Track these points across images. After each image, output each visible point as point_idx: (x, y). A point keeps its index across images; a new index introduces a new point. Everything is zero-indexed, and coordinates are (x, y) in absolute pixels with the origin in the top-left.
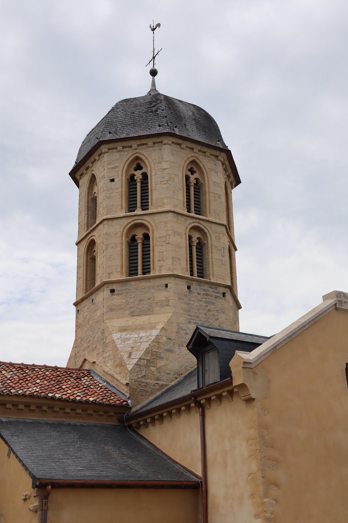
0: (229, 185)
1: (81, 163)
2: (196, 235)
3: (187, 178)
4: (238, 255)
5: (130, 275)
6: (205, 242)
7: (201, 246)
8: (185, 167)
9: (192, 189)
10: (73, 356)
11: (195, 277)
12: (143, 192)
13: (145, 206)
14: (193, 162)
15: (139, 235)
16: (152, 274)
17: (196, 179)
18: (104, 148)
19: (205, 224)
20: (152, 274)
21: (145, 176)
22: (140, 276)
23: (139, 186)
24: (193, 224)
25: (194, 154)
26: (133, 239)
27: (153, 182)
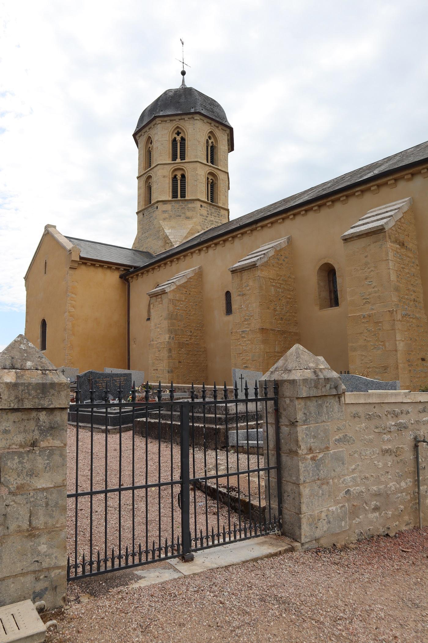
1: (140, 202)
2: (210, 177)
3: (207, 142)
5: (173, 160)
7: (213, 184)
8: (206, 135)
10: (138, 240)
11: (210, 202)
12: (181, 154)
13: (183, 157)
14: (211, 132)
16: (186, 161)
17: (212, 142)
18: (158, 121)
19: (216, 170)
20: (186, 161)
21: (183, 139)
22: (179, 198)
23: (179, 182)
24: (210, 171)
25: (212, 128)
26: (175, 178)
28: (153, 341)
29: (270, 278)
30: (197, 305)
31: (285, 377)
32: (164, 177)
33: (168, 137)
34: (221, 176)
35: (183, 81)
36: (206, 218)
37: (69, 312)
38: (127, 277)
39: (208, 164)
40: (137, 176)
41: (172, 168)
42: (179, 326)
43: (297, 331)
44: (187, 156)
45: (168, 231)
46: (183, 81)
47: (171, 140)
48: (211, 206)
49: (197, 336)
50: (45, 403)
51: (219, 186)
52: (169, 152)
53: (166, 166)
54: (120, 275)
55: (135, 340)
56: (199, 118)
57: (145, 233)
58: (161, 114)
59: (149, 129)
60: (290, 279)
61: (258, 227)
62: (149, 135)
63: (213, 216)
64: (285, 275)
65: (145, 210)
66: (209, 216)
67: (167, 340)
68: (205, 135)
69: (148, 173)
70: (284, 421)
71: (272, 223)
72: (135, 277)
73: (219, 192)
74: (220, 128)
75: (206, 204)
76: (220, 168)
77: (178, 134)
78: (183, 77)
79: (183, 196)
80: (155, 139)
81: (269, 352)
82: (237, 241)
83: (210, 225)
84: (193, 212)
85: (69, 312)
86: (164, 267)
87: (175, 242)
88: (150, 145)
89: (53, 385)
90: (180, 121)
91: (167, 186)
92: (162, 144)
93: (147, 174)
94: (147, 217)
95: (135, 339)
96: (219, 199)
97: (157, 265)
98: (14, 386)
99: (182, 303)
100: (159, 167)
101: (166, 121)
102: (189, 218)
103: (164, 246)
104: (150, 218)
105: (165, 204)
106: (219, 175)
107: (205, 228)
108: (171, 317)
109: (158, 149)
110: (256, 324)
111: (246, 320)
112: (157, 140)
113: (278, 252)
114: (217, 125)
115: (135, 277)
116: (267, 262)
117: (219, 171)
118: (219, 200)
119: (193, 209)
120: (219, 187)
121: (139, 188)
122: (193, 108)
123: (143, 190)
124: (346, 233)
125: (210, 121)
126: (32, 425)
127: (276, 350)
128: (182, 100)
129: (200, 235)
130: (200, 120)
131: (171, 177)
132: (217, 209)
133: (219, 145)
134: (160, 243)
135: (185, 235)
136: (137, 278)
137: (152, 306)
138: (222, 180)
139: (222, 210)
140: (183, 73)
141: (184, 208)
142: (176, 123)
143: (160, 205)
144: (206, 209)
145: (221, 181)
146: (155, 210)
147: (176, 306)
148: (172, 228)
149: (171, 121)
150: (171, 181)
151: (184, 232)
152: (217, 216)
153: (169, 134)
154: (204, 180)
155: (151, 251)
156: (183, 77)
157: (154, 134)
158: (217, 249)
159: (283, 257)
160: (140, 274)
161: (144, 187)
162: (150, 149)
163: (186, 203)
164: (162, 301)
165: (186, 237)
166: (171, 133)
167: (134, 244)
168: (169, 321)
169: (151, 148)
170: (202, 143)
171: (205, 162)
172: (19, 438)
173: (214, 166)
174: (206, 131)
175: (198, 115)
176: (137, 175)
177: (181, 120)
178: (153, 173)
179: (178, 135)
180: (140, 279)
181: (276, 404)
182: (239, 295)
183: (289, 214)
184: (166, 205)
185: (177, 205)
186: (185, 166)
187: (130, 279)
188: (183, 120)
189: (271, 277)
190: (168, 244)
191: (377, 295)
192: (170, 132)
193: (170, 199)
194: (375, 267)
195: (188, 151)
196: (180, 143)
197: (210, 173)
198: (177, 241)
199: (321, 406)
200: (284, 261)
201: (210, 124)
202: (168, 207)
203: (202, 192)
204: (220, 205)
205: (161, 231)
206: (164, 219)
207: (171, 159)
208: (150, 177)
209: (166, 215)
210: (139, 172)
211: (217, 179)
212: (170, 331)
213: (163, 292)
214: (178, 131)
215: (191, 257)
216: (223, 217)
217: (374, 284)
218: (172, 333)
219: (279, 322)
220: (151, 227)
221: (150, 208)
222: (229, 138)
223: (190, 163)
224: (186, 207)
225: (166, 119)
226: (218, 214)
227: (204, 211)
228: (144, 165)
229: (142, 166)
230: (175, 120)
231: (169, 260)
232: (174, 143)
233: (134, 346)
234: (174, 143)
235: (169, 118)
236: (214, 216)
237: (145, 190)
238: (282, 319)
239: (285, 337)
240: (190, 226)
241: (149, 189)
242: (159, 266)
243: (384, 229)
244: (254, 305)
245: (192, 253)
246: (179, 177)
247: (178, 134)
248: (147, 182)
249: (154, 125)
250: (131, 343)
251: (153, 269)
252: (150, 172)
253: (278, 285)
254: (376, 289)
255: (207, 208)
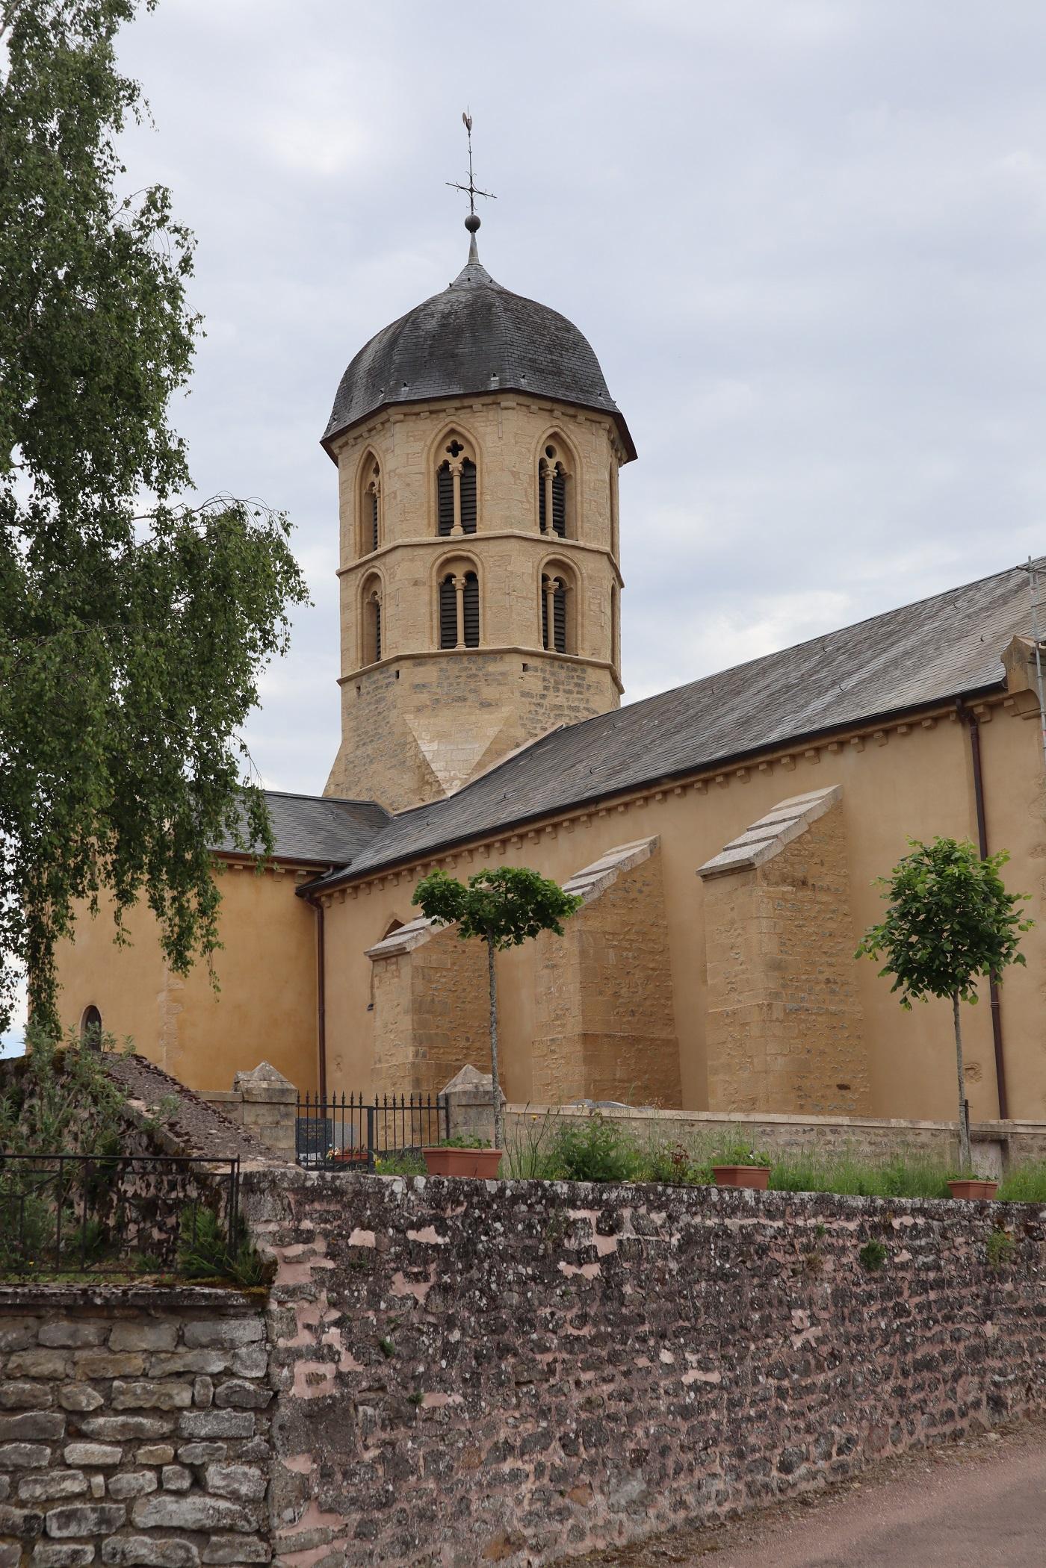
0: (615, 461)
1: (348, 649)
2: (553, 574)
3: (542, 465)
4: (624, 594)
6: (572, 473)
7: (564, 592)
9: (551, 599)
10: (345, 765)
13: (469, 525)
14: (554, 436)
15: (459, 572)
16: (478, 534)
17: (558, 466)
18: (394, 414)
19: (568, 552)
20: (478, 534)
21: (468, 465)
22: (461, 647)
24: (552, 557)
25: (555, 422)
27: (484, 481)
28: (380, 1061)
29: (605, 933)
30: (481, 976)
31: (453, 1090)
32: (416, 583)
33: (424, 463)
34: (588, 568)
35: (473, 251)
36: (542, 701)
37: (170, 991)
38: (317, 895)
39: (544, 537)
40: (338, 567)
41: (439, 557)
42: (438, 1027)
43: (672, 1037)
44: (481, 519)
45: (428, 748)
46: (473, 251)
47: (433, 469)
48: (556, 663)
49: (482, 1049)
50: (284, 1100)
51: (579, 597)
52: (429, 507)
53: (421, 551)
54: (297, 888)
55: (339, 1059)
56: (513, 404)
57: (364, 744)
58: (404, 393)
59: (370, 431)
60: (655, 929)
61: (602, 810)
62: (370, 448)
63: (561, 693)
64: (642, 922)
65: (364, 678)
66: (551, 693)
67: (410, 1059)
68: (533, 450)
69: (370, 564)
70: (451, 1125)
71: (626, 805)
72: (336, 895)
73: (580, 618)
74: (581, 418)
75: (539, 659)
76: (581, 543)
77: (455, 449)
78: (473, 239)
79: (472, 639)
80: (389, 463)
81: (600, 1081)
82: (562, 835)
83: (552, 721)
84: (500, 687)
85: (170, 991)
86: (409, 878)
87: (447, 782)
88: (372, 477)
89: (288, 1090)
90: (460, 412)
91: (424, 610)
92: (408, 485)
93: (367, 566)
94: (368, 697)
95: (339, 1056)
96: (580, 638)
97: (390, 872)
98: (267, 1090)
99: (445, 973)
100: (399, 553)
101: (418, 414)
102: (490, 705)
103: (418, 791)
104: (378, 702)
105: (420, 664)
106: (579, 563)
107: (538, 731)
108: (420, 1007)
109: (395, 498)
110: (574, 1026)
111: (557, 1018)
112: (394, 471)
113: (627, 875)
114: (571, 411)
115: (336, 895)
116: (599, 899)
117: (578, 551)
118: (579, 642)
119: (500, 678)
120: (580, 601)
121: (344, 607)
122: (495, 375)
123: (355, 615)
124: (704, 867)
125: (548, 405)
126: (276, 1112)
127: (618, 1076)
128: (464, 349)
129: (521, 754)
130: (518, 407)
131: (435, 584)
132: (575, 670)
133: (578, 470)
134: (408, 780)
135: (477, 758)
136: (343, 898)
137: (376, 980)
138: (590, 578)
139: (590, 670)
140: (473, 225)
141: (476, 675)
142: (447, 420)
143: (405, 668)
144: (539, 674)
145: (586, 582)
146: (390, 680)
147: (430, 981)
148: (441, 736)
149: (431, 412)
150: (436, 595)
151: (475, 750)
152: (576, 689)
153: (428, 454)
154: (534, 588)
155: (383, 802)
156: (473, 239)
157: (384, 448)
158: (524, 849)
159: (638, 885)
160: (349, 891)
161: (359, 606)
162: (375, 489)
163: (480, 660)
164: (398, 970)
165: (480, 765)
166: (433, 450)
167: (332, 773)
168: (415, 1017)
169: (377, 486)
170: (525, 478)
171: (536, 533)
172: (270, 1119)
173: (563, 541)
174: (537, 436)
175: (511, 396)
176: (337, 567)
177: (463, 411)
178: (382, 567)
179: (455, 455)
180: (350, 903)
181: (447, 1112)
182: (547, 967)
183: (654, 791)
184: (421, 669)
185: (453, 668)
186: (477, 551)
187: (323, 899)
188: (468, 410)
189: (607, 929)
190: (430, 784)
191: (744, 977)
192: (430, 449)
193: (435, 649)
194: (744, 928)
195: (482, 506)
196: (462, 476)
197: (554, 563)
198: (453, 779)
199: (480, 1113)
200: (641, 892)
201: (551, 411)
202: (428, 673)
203: (528, 627)
204: (583, 656)
205: (408, 746)
206: (419, 710)
207: (434, 529)
208: (373, 578)
209: (424, 698)
210: (344, 559)
211: (575, 576)
212: (417, 1040)
213: (401, 952)
214: (454, 443)
215: (469, 859)
216: (592, 691)
217: (742, 959)
218: (420, 1044)
219: (625, 1020)
220: (380, 731)
221: (378, 672)
222: (615, 434)
223: (491, 541)
224: (480, 674)
225: (417, 409)
226: (577, 685)
227: (533, 682)
228: (358, 539)
229: (352, 541)
230: (444, 410)
231: (420, 862)
232: (443, 477)
233: (339, 1074)
234: (443, 477)
235: (425, 407)
236: (564, 691)
237: (362, 614)
238: (633, 1013)
239: (640, 1050)
240: (492, 732)
241: (374, 609)
242: (397, 875)
243: (753, 864)
244: (571, 988)
245: (471, 852)
246: (459, 582)
247: (455, 449)
248: (368, 590)
249: (383, 423)
250: (330, 1066)
251: (383, 880)
252: (376, 563)
253: (625, 944)
254: (743, 967)
255: (543, 671)
